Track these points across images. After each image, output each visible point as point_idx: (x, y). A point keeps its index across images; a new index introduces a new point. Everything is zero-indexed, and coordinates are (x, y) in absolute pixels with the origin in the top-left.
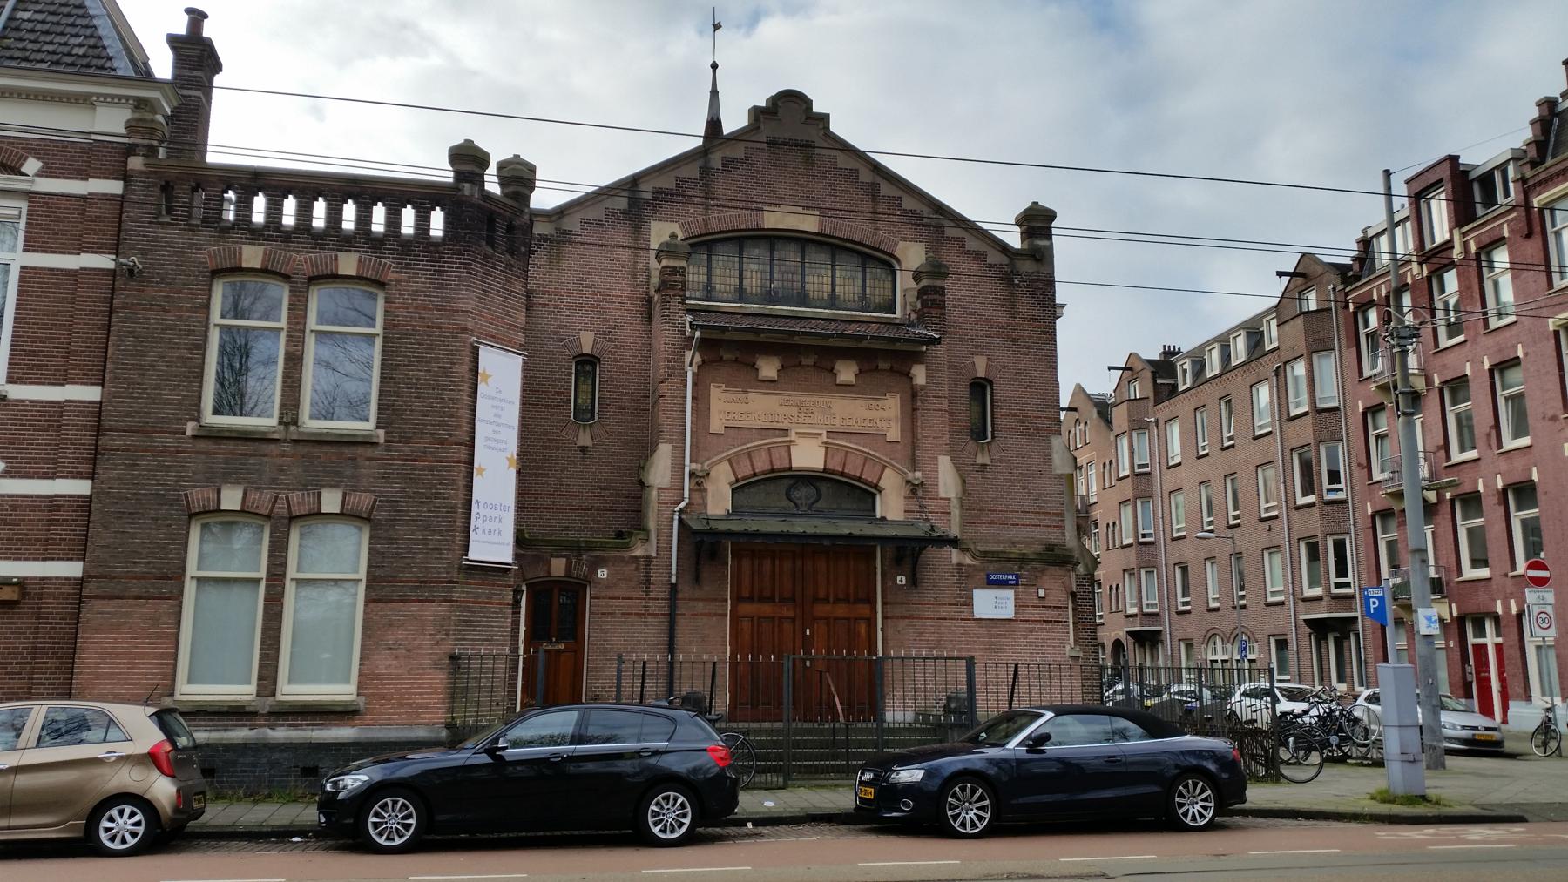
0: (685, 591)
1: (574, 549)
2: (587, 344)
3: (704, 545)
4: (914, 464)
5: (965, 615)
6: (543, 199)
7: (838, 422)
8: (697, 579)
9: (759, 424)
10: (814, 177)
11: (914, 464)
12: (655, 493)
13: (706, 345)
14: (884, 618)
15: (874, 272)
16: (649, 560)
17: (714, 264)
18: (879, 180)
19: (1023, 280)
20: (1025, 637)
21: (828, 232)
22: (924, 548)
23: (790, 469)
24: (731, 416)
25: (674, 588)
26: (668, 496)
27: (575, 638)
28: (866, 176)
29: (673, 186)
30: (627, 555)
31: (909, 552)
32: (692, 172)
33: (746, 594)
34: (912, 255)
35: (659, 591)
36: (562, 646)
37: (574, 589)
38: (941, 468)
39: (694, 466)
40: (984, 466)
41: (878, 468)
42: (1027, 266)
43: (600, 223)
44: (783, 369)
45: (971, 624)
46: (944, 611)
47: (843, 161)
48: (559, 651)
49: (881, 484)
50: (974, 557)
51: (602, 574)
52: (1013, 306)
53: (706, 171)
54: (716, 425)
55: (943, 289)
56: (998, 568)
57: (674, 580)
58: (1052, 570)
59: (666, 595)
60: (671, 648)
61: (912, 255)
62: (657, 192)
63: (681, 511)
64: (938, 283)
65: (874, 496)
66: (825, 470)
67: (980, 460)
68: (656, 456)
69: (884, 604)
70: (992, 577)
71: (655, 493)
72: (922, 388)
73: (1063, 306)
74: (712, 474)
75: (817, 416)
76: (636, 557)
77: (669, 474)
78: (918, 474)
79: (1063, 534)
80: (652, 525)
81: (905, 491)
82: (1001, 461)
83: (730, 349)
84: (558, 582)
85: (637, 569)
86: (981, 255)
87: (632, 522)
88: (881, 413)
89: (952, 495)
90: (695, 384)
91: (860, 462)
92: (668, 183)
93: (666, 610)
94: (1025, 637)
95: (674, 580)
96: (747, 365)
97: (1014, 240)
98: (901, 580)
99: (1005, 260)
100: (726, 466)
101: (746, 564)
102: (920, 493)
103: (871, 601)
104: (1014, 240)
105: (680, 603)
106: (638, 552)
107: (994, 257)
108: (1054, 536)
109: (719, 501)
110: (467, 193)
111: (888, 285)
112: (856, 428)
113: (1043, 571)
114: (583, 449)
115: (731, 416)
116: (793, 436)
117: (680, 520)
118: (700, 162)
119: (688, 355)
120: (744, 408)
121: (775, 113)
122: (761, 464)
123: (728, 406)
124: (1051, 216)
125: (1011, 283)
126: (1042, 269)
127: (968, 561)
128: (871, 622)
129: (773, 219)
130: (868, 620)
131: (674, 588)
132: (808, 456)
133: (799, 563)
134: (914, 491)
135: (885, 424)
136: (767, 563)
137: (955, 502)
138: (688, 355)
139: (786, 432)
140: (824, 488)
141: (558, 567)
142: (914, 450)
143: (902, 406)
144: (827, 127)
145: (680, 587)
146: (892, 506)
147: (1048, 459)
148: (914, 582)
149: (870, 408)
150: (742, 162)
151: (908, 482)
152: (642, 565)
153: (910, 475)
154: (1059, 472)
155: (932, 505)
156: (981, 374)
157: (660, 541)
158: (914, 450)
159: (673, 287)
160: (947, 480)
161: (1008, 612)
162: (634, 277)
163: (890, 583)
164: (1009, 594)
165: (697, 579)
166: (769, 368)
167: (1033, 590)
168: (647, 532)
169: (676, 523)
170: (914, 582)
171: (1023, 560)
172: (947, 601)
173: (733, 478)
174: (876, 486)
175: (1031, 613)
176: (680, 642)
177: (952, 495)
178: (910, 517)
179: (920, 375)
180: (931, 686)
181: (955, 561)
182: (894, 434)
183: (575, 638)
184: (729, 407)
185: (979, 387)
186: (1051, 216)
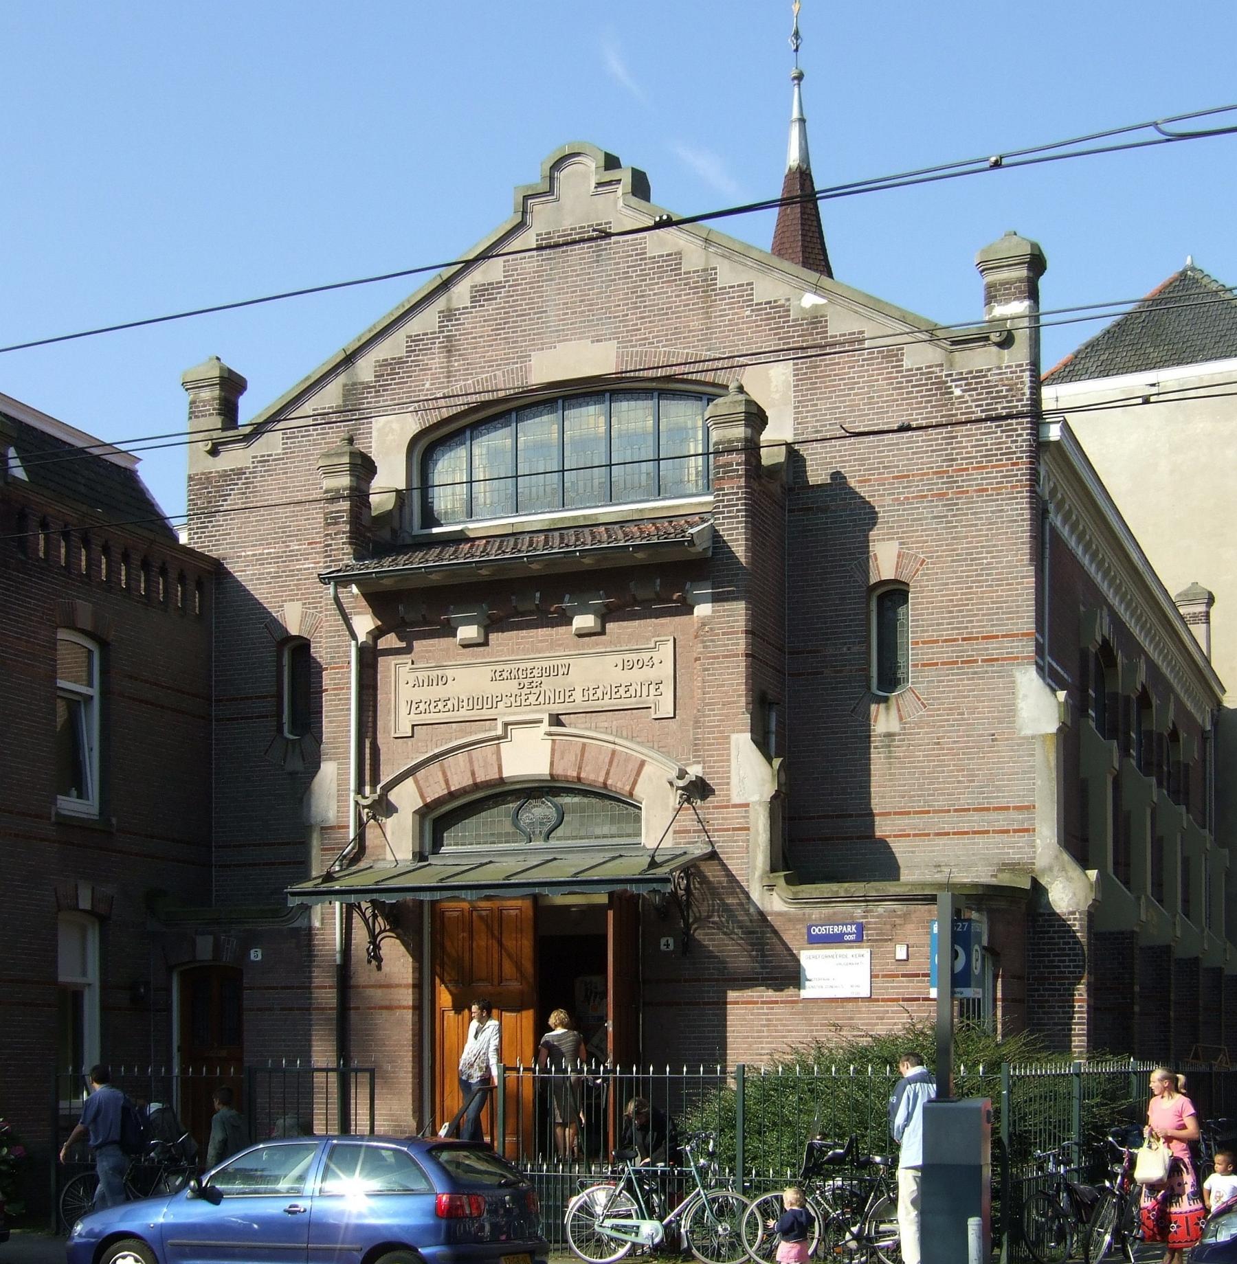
18: (717, 262)
40: (889, 735)
44: (606, 616)
70: (816, 931)
81: (674, 799)
120: (438, 692)
122: (460, 780)
129: (547, 367)
132: (526, 757)
141: (204, 948)
147: (1009, 712)
149: (627, 666)
150: (498, 286)
154: (1028, 732)
167: (888, 946)
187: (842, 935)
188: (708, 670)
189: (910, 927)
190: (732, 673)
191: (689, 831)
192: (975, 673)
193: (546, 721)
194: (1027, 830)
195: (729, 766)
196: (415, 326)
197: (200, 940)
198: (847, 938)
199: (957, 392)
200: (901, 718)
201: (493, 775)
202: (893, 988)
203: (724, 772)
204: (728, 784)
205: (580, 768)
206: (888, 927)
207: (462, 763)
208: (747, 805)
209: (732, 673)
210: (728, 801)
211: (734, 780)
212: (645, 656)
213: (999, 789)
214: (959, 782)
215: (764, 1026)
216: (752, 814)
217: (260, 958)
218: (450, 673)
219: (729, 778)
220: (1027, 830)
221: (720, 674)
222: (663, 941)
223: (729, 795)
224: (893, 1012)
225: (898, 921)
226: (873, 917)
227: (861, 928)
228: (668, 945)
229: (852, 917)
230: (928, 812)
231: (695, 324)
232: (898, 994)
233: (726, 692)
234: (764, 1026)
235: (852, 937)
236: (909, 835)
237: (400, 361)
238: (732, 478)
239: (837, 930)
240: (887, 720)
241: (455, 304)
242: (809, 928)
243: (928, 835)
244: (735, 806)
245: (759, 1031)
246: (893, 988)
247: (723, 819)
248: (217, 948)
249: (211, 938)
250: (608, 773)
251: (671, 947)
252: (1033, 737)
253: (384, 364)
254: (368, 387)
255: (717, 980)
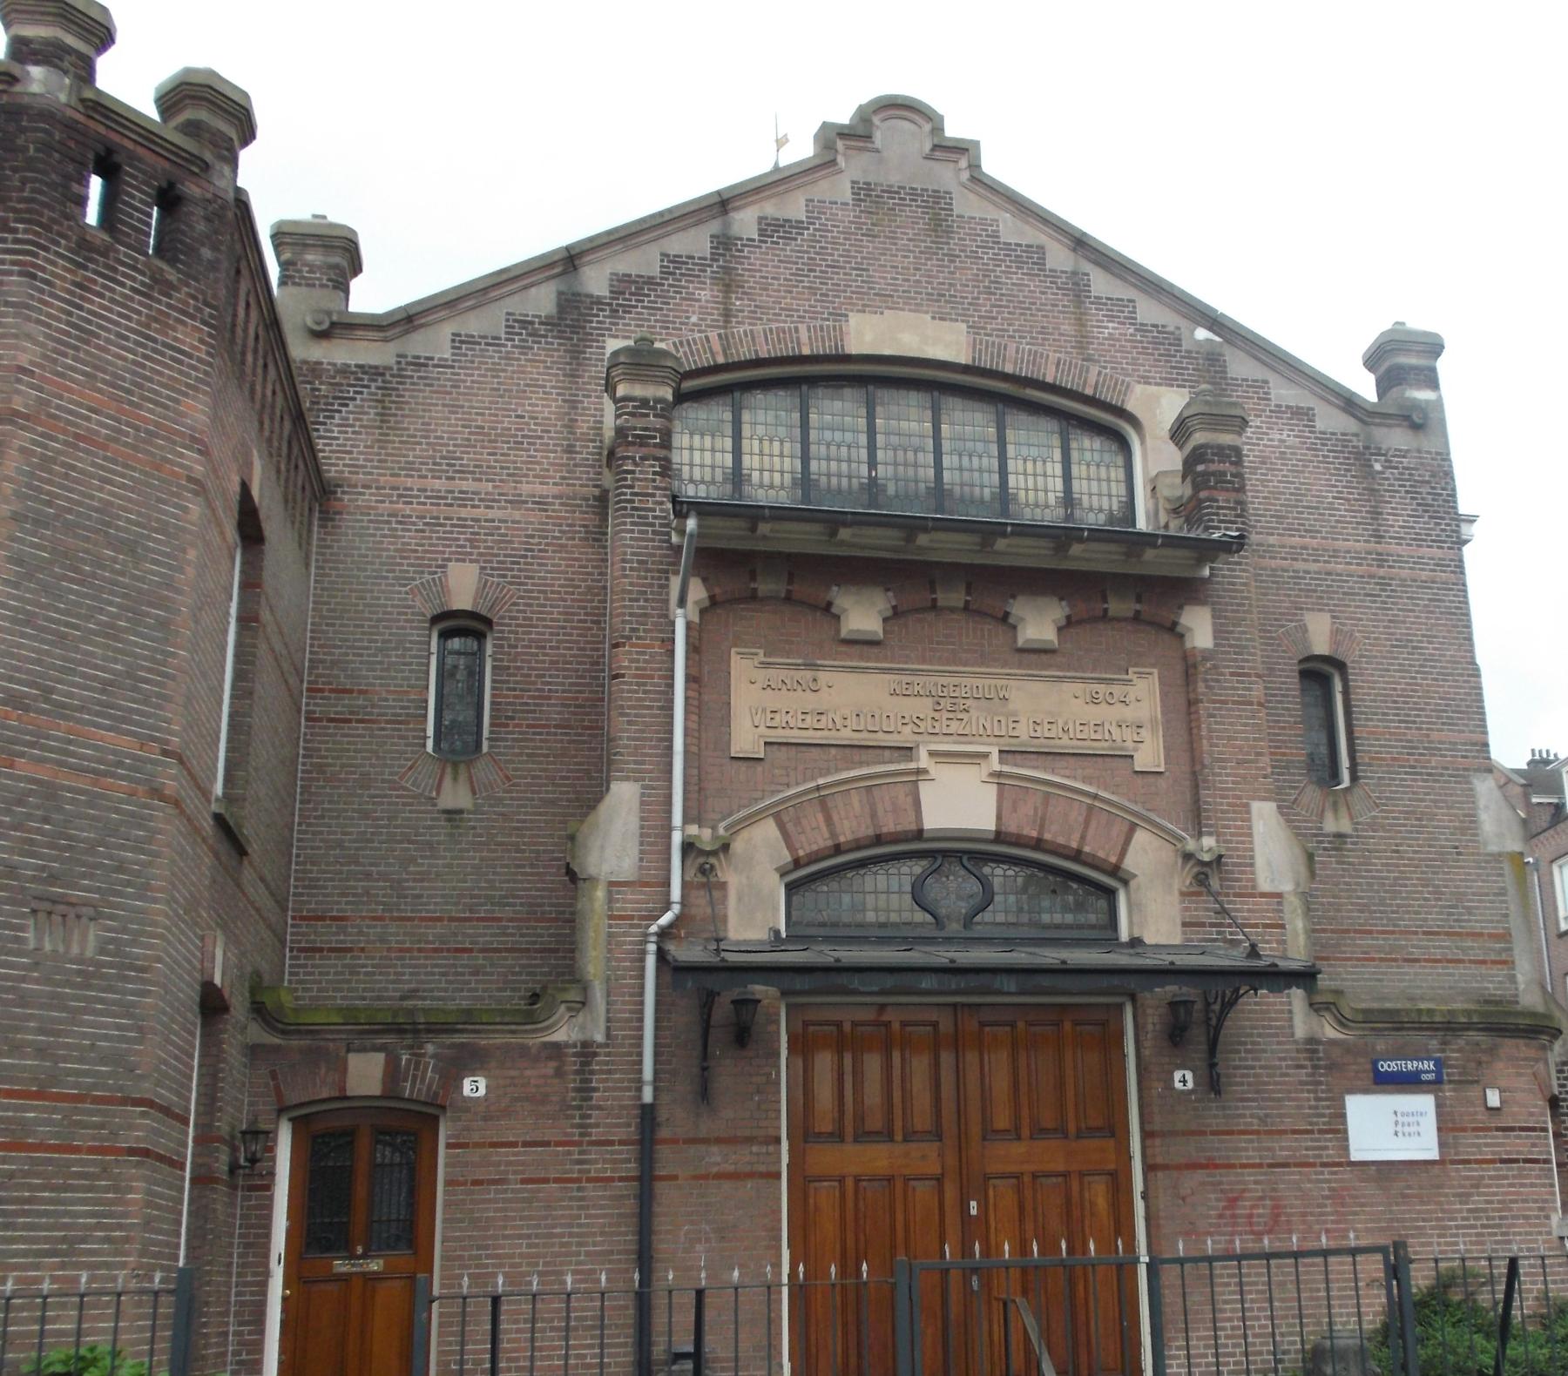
0: (676, 1120)
1: (399, 1028)
2: (463, 588)
3: (716, 1004)
4: (1198, 820)
5: (1331, 1154)
6: (370, 295)
7: (1024, 731)
8: (704, 1093)
9: (846, 736)
10: (953, 257)
11: (1198, 820)
12: (600, 894)
13: (712, 560)
14: (1149, 1168)
15: (1087, 447)
16: (587, 1051)
17: (746, 430)
18: (1087, 267)
19: (1388, 465)
20: (1464, 1197)
21: (986, 362)
22: (1229, 1005)
23: (919, 834)
24: (779, 719)
25: (648, 1116)
26: (630, 902)
27: (411, 1243)
28: (1060, 258)
29: (655, 271)
30: (534, 1041)
31: (1203, 1005)
32: (696, 242)
33: (825, 1125)
34: (1160, 406)
35: (613, 1123)
36: (375, 1266)
37: (408, 1127)
38: (1259, 827)
39: (693, 830)
41: (1118, 830)
42: (1396, 438)
43: (495, 341)
44: (1067, 626)
45: (1346, 1174)
46: (1283, 1148)
47: (1011, 229)
48: (370, 1278)
49: (1129, 863)
50: (1342, 1022)
51: (474, 1087)
52: (1376, 514)
53: (724, 243)
54: (745, 737)
55: (1237, 451)
56: (1393, 1047)
57: (648, 1096)
58: (1509, 1046)
59: (631, 1132)
60: (645, 1258)
61: (1160, 406)
62: (627, 287)
63: (664, 934)
64: (1227, 439)
65: (1110, 894)
66: (999, 837)
67: (1330, 826)
68: (603, 807)
69: (1146, 1135)
70: (1386, 1066)
71: (600, 894)
72: (1207, 655)
73: (1471, 520)
74: (738, 846)
75: (977, 717)
76: (556, 1046)
77: (633, 850)
78: (1208, 842)
79: (1513, 979)
80: (594, 963)
81: (1182, 879)
82: (1373, 826)
83: (771, 569)
84: (366, 1107)
85: (559, 1073)
86: (1302, 415)
87: (554, 972)
88: (1118, 712)
89: (1287, 887)
90: (693, 649)
91: (1076, 816)
92: (643, 261)
93: (632, 1168)
94: (1464, 1197)
95: (648, 1096)
96: (814, 607)
97: (1365, 387)
98: (1184, 1079)
99: (1351, 425)
100: (767, 831)
101: (824, 1062)
102: (1215, 883)
103: (1115, 1130)
104: (1365, 387)
105: (664, 1152)
106: (560, 1036)
107: (1331, 420)
108: (1491, 983)
109: (755, 912)
110: (35, 88)
111: (1118, 474)
112: (1065, 744)
113: (1492, 1051)
114: (452, 814)
115: (779, 719)
116: (924, 761)
117: (661, 955)
118: (714, 227)
119: (675, 583)
120: (810, 701)
121: (868, 137)
123: (767, 699)
124: (1433, 347)
125: (1369, 474)
126: (1426, 446)
127: (1330, 1032)
128: (1119, 1183)
129: (867, 334)
130: (1113, 1175)
131: (648, 1116)
132: (959, 802)
133: (947, 1058)
134: (1201, 880)
135: (1129, 735)
136: (873, 1064)
137: (1293, 905)
138: (675, 583)
139: (907, 751)
140: (998, 875)
141: (365, 1074)
142: (1196, 787)
143: (1164, 695)
144: (975, 166)
145: (663, 1115)
146: (1154, 917)
147: (1470, 823)
148: (1212, 1083)
149: (1094, 701)
150: (799, 226)
151: (1188, 856)
152: (572, 1064)
153: (1191, 845)
155: (1242, 909)
156: (1321, 647)
157: (619, 1008)
158: (1196, 787)
159: (642, 441)
160: (1270, 850)
161: (1423, 1145)
162: (570, 450)
163: (1159, 1088)
164: (1423, 1105)
165: (704, 1093)
166: (862, 614)
167: (1473, 1093)
168: (585, 988)
169: (651, 962)
170: (1212, 1083)
171: (1449, 1027)
172: (1288, 1123)
173: (786, 857)
174: (1115, 871)
175: (1474, 1146)
176: (663, 1244)
177: (1287, 887)
178: (1196, 936)
179: (1199, 628)
180: (1260, 1324)
181: (1300, 1031)
182: (1150, 754)
183: (411, 1243)
184: (771, 700)
185: (1319, 675)
186: (1433, 347)
187: (1418, 1073)
188: (1214, 716)
189: (1500, 1065)
190: (1246, 725)
191: (1203, 925)
192: (1429, 774)
193: (995, 756)
194: (1504, 962)
195: (1251, 842)
196: (678, 244)
197: (356, 1062)
198: (1424, 1077)
199: (1378, 467)
200: (1351, 818)
201: (908, 825)
202: (1487, 1145)
203: (1246, 850)
204: (1252, 865)
205: (1042, 826)
206: (1473, 1065)
207: (856, 804)
208: (1279, 895)
209: (1246, 725)
210: (1254, 887)
211: (1260, 861)
212: (1117, 690)
213: (1469, 910)
214: (1425, 899)
215: (1327, 1197)
216: (1286, 908)
217: (482, 1092)
218: (823, 677)
219: (1252, 857)
220: (1504, 962)
221: (1231, 724)
222: (1178, 1075)
223: (1253, 880)
224: (1491, 1178)
225: (1484, 1058)
226: (1453, 1051)
227: (1439, 1064)
228: (1184, 1082)
229: (1428, 1051)
230: (1393, 932)
231: (1066, 328)
232: (1493, 1153)
233: (1240, 747)
234: (1327, 1197)
235: (1431, 1077)
236: (1373, 959)
237: (650, 281)
238: (1227, 490)
239: (1411, 1066)
240: (1337, 819)
241: (736, 230)
242: (1375, 1063)
243: (1395, 960)
244: (1263, 895)
245: (1319, 1206)
246: (1487, 1145)
247: (1249, 911)
248: (393, 1073)
249: (380, 1057)
250: (1083, 838)
251: (1190, 1085)
252: (1500, 854)
253: (626, 279)
254: (598, 301)
255: (1257, 1132)
